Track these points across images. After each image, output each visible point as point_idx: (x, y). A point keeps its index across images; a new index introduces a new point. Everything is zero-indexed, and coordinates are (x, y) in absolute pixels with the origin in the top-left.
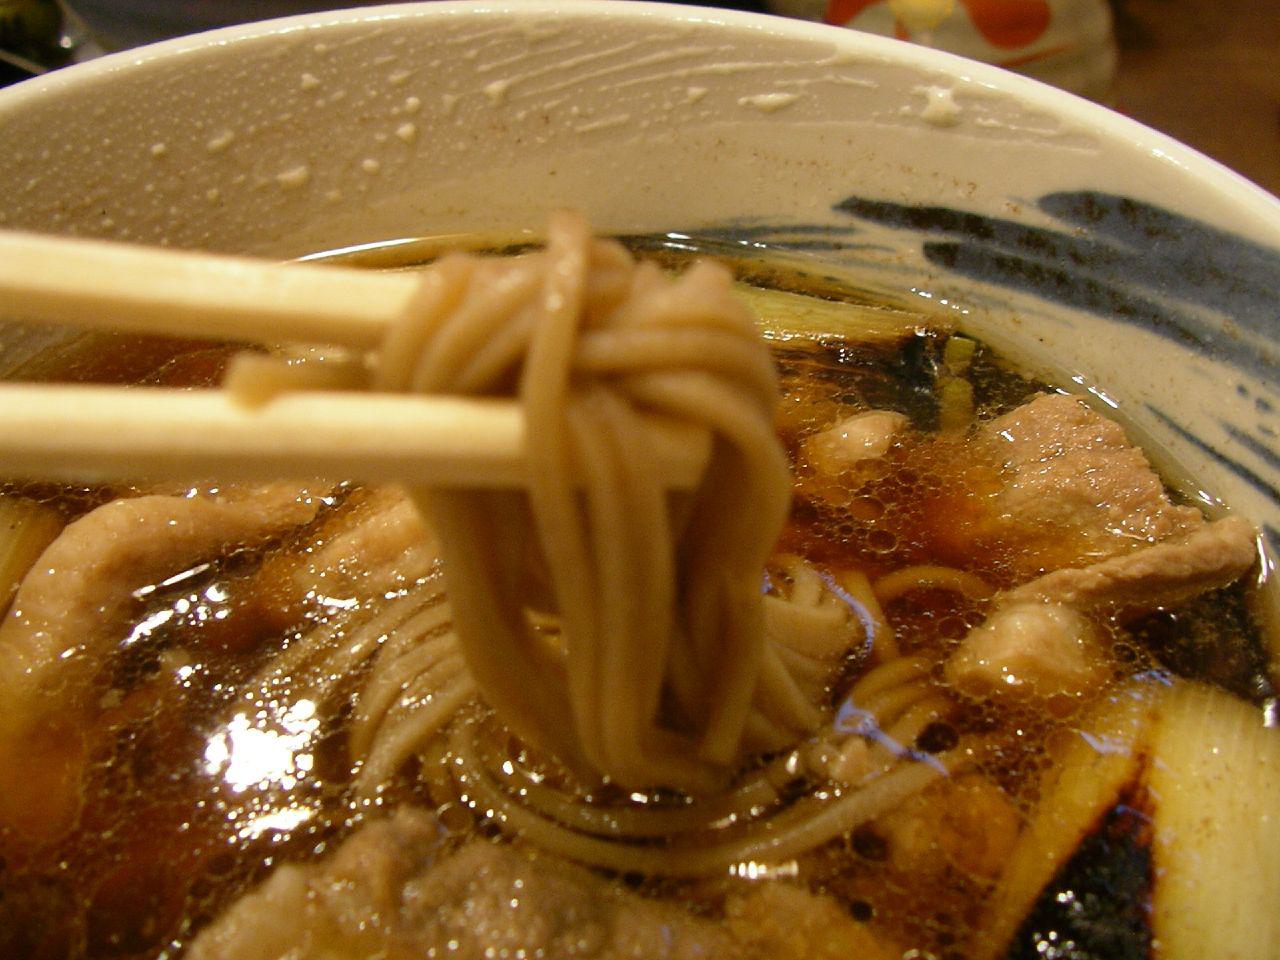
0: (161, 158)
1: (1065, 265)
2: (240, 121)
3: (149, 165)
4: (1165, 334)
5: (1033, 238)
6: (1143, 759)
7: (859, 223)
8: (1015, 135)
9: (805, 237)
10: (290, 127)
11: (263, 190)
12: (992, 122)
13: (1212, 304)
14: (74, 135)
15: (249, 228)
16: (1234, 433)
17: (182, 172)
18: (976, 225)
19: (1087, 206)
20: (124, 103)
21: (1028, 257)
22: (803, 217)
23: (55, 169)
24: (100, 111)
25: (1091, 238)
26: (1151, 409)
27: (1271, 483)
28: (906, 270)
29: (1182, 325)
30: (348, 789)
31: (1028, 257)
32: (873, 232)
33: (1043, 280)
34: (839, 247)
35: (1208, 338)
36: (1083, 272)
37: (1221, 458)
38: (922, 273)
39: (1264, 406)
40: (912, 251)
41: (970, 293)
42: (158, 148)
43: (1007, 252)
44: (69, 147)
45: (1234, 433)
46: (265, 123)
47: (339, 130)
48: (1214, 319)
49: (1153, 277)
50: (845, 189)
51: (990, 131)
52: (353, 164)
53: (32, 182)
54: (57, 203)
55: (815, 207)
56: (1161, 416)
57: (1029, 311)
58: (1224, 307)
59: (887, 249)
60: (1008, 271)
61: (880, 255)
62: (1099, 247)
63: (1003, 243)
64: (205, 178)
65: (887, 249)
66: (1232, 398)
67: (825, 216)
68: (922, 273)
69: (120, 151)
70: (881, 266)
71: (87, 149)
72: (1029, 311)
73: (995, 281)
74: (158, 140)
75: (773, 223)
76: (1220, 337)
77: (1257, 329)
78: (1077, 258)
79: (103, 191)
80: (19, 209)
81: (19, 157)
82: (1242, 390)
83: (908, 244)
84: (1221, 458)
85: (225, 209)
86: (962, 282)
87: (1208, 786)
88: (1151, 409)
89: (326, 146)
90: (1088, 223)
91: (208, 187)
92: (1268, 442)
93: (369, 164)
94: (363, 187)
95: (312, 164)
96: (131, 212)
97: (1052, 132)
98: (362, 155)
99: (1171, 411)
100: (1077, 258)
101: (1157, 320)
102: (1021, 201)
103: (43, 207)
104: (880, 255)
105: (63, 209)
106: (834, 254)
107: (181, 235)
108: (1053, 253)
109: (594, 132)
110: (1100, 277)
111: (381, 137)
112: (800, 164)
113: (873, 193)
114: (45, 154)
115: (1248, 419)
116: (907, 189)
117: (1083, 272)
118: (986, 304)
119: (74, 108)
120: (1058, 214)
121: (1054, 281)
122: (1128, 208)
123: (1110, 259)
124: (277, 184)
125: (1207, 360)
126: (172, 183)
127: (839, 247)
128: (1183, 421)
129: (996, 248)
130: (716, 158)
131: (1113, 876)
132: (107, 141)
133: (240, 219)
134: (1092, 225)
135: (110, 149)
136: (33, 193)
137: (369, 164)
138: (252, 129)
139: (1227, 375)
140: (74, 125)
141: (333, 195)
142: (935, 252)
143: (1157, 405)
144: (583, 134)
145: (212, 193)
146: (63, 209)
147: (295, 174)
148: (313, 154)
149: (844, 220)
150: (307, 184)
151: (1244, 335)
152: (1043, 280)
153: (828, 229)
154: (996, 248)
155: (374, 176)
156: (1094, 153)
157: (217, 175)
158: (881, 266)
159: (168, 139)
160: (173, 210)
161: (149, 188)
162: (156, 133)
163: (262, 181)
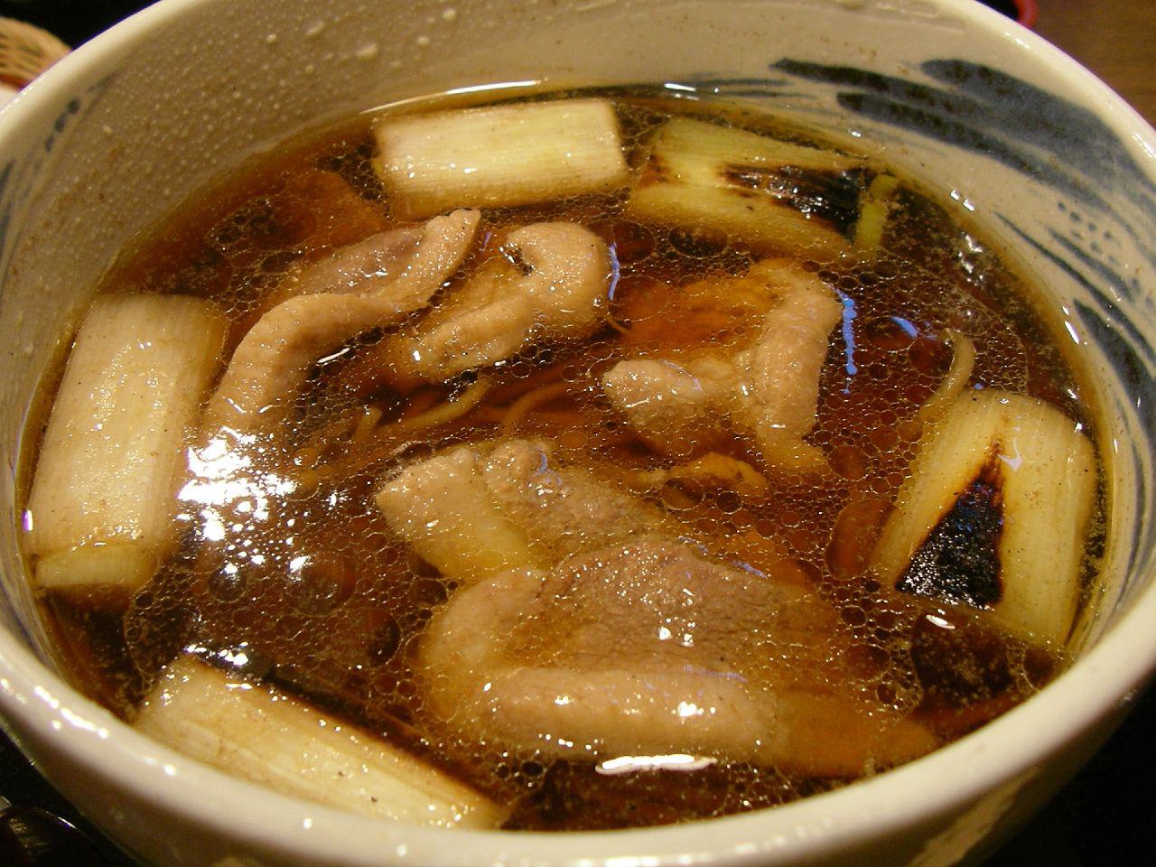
0: (274, 45)
1: (940, 112)
2: (329, 14)
3: (266, 51)
4: (1011, 165)
5: (917, 92)
6: (997, 449)
7: (789, 78)
8: (905, 17)
9: (752, 87)
10: (365, 16)
11: (345, 64)
12: (888, 7)
13: (1042, 144)
14: (214, 33)
15: (336, 92)
16: (1055, 235)
17: (289, 54)
18: (876, 81)
19: (956, 70)
20: (247, 7)
21: (913, 105)
22: (748, 73)
23: (201, 59)
24: (231, 13)
25: (958, 93)
26: (1000, 217)
27: (1079, 271)
28: (823, 112)
29: (1022, 158)
30: (722, 619)
31: (913, 105)
32: (799, 84)
33: (924, 121)
34: (774, 95)
35: (1039, 169)
36: (953, 117)
37: (1046, 253)
38: (836, 115)
39: (1075, 217)
40: (828, 99)
41: (871, 130)
42: (272, 37)
43: (898, 102)
44: (210, 42)
45: (1055, 235)
46: (347, 14)
47: (400, 17)
48: (1044, 155)
49: (1006, 124)
50: (779, 53)
51: (889, 13)
52: (410, 41)
53: (186, 70)
54: (203, 84)
55: (757, 64)
56: (1007, 222)
57: (915, 144)
58: (1050, 147)
59: (810, 97)
60: (899, 115)
61: (805, 101)
62: (964, 101)
63: (897, 95)
64: (305, 58)
65: (810, 97)
66: (1055, 211)
67: (763, 72)
68: (836, 115)
69: (246, 43)
70: (808, 109)
71: (222, 42)
72: (915, 144)
73: (889, 121)
74: (272, 32)
75: (725, 77)
76: (1047, 169)
77: (1072, 163)
78: (949, 107)
79: (234, 72)
80: (178, 90)
81: (177, 52)
82: (1061, 206)
83: (826, 94)
84: (1046, 253)
85: (319, 80)
86: (866, 122)
87: (1038, 470)
88: (1000, 217)
89: (391, 29)
90: (957, 83)
91: (306, 63)
92: (1077, 242)
93: (423, 40)
94: (417, 58)
95: (381, 43)
96: (253, 87)
97: (931, 16)
98: (417, 34)
99: (1013, 218)
100: (949, 107)
101: (1005, 154)
102: (908, 64)
103: (195, 87)
104: (805, 101)
105: (207, 88)
106: (770, 100)
107: (287, 101)
108: (932, 103)
109: (589, 11)
110: (965, 123)
111: (431, 20)
112: (746, 34)
113: (800, 55)
114: (195, 49)
115: (1064, 225)
116: (825, 54)
117: (953, 117)
118: (882, 139)
119: (213, 14)
120: (936, 77)
121: (932, 124)
122: (985, 73)
123: (972, 109)
124: (355, 59)
125: (1038, 183)
126: (281, 62)
127: (774, 95)
128: (1021, 226)
129: (890, 98)
130: (682, 30)
131: (546, 765)
132: (236, 36)
133: (329, 86)
134: (960, 85)
135: (238, 41)
136: (187, 78)
137: (423, 40)
138: (337, 19)
139: (1051, 195)
140: (213, 25)
141: (396, 64)
142: (845, 100)
143: (1003, 214)
144: (581, 13)
145: (310, 68)
146: (207, 88)
147: (369, 50)
148: (382, 35)
149: (778, 75)
150: (380, 54)
151: (1063, 167)
152: (924, 121)
153: (766, 82)
154: (890, 98)
155: (425, 49)
156: (960, 32)
157: (313, 54)
158: (808, 109)
159: (278, 30)
160: (282, 83)
161: (266, 67)
162: (270, 27)
163: (345, 56)
